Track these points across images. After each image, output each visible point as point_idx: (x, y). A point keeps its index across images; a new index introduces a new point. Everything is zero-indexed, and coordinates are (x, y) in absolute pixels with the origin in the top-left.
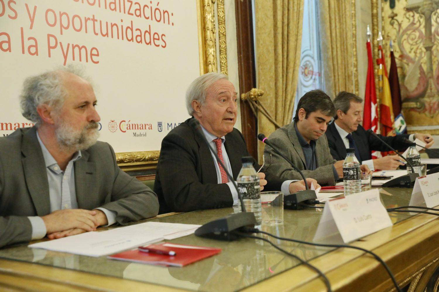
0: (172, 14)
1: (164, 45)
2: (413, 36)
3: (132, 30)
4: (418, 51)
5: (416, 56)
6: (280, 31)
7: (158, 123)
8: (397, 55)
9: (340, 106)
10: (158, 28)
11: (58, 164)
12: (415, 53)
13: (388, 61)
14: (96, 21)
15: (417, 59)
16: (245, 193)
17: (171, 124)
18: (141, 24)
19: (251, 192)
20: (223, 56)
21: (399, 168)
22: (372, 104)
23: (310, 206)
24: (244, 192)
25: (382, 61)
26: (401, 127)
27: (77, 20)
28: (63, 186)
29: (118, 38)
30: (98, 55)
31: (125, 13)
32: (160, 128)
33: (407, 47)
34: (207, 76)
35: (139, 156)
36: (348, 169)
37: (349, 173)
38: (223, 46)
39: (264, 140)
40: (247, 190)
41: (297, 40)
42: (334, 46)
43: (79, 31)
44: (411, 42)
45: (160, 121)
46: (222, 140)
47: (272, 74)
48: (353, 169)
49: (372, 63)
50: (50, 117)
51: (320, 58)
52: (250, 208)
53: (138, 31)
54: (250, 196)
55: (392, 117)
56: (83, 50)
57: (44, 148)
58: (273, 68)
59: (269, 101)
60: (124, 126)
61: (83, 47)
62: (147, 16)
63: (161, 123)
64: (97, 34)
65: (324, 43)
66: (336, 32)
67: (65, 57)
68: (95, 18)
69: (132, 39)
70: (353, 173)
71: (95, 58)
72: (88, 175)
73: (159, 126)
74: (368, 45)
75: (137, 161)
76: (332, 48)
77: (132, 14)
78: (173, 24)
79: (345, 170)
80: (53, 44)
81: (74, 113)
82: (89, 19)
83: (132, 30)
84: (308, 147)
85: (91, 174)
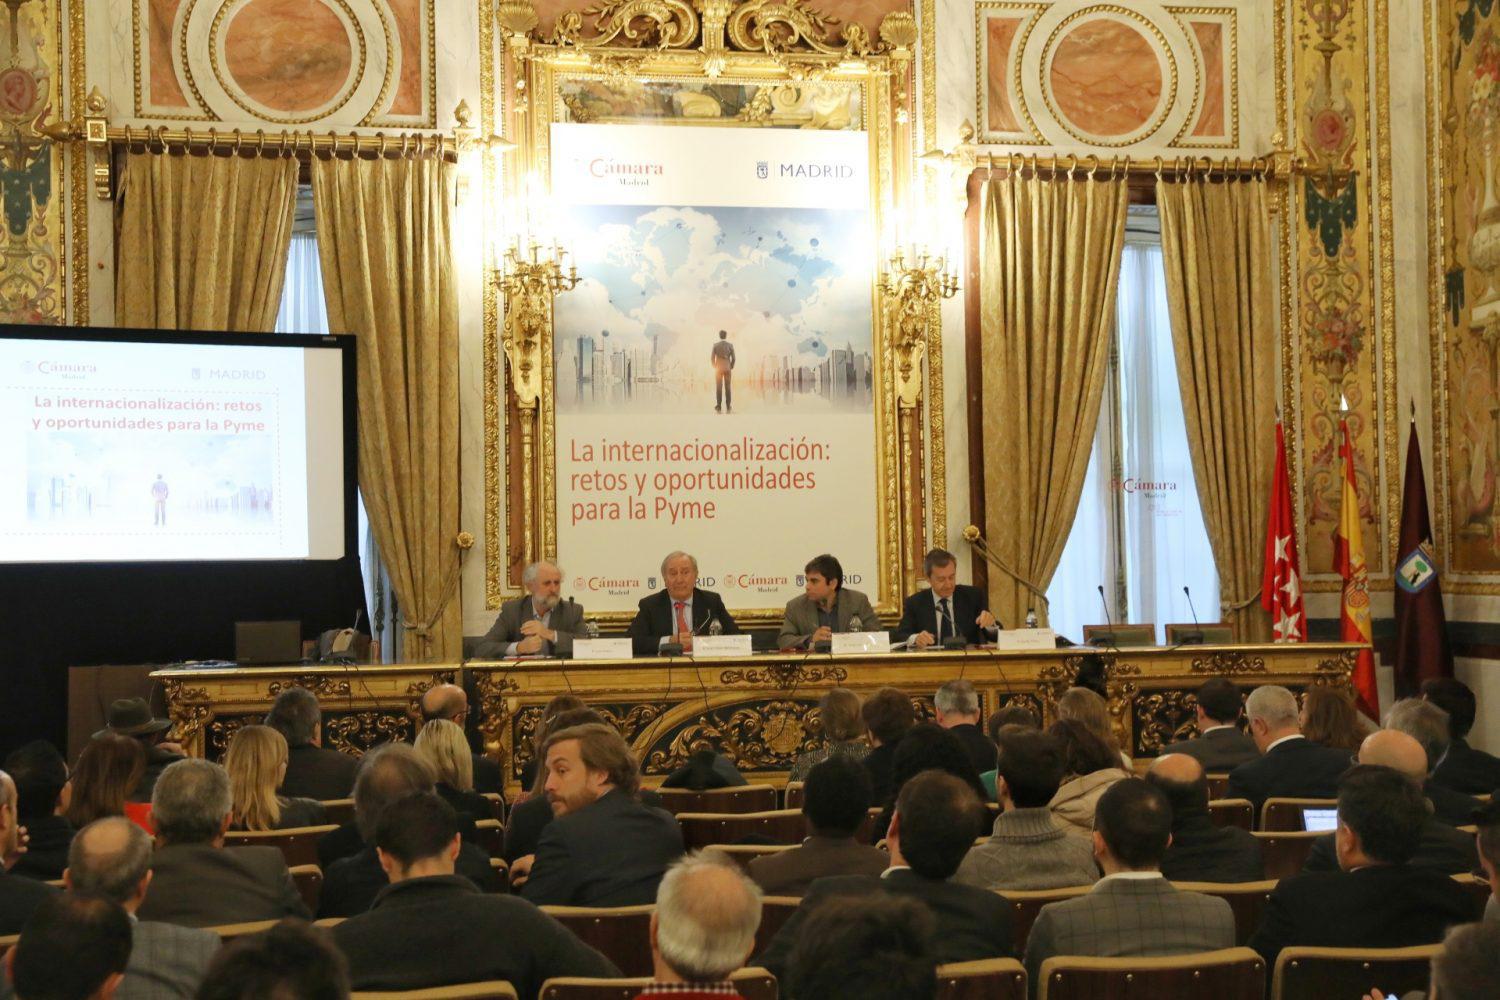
1: (811, 484)
9: (443, 740)
18: (777, 467)
22: (1277, 541)
26: (1416, 577)
35: (756, 613)
56: (696, 508)
59: (1002, 541)
60: (745, 581)
67: (675, 517)
71: (709, 513)
75: (757, 618)
81: (542, 586)
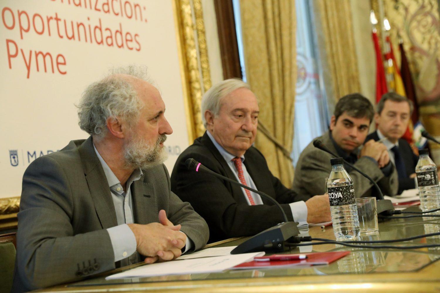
0: (145, 8)
2: (424, 23)
3: (101, 29)
4: (433, 41)
5: (430, 48)
6: (271, 23)
7: (11, 151)
8: (407, 48)
10: (130, 26)
11: (121, 184)
12: (429, 43)
13: (397, 55)
14: (60, 20)
15: (432, 51)
16: (340, 197)
17: (35, 153)
19: (347, 197)
20: (204, 59)
24: (338, 197)
25: (391, 55)
27: (38, 20)
28: (125, 209)
29: (86, 41)
30: (65, 64)
31: (91, 8)
32: (15, 161)
33: (418, 37)
34: (226, 84)
36: (424, 174)
38: (203, 46)
40: (342, 195)
41: (291, 34)
42: (333, 40)
43: (41, 33)
44: (422, 30)
45: (13, 148)
46: (242, 159)
47: (267, 78)
48: (429, 173)
49: (381, 58)
50: (121, 131)
51: (314, 54)
52: (363, 207)
53: (108, 31)
54: (346, 201)
57: (106, 166)
58: (267, 71)
61: (48, 54)
62: (116, 12)
63: (16, 151)
64: (61, 37)
65: (320, 37)
66: (334, 22)
67: (29, 68)
68: (59, 17)
69: (102, 42)
71: (62, 68)
72: (145, 198)
73: (12, 157)
74: (375, 37)
76: (331, 43)
77: (99, 10)
78: (146, 21)
79: (420, 175)
80: (13, 52)
81: (148, 125)
82: (51, 18)
83: (101, 29)
85: (149, 196)
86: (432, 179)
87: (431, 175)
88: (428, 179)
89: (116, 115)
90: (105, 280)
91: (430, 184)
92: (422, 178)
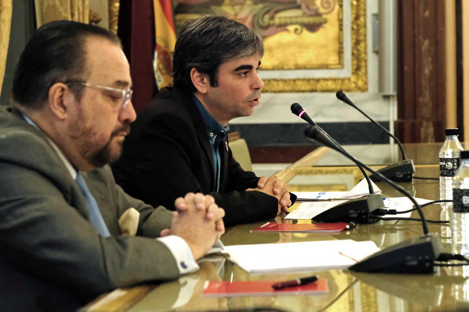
21: (463, 143)
23: (383, 217)
37: (447, 166)
39: (300, 115)
55: (387, 131)
70: (452, 165)
84: (388, 142)
86: (454, 169)
87: (453, 163)
88: (449, 168)
89: (165, 53)
90: (117, 2)
91: (451, 175)
92: (443, 166)
